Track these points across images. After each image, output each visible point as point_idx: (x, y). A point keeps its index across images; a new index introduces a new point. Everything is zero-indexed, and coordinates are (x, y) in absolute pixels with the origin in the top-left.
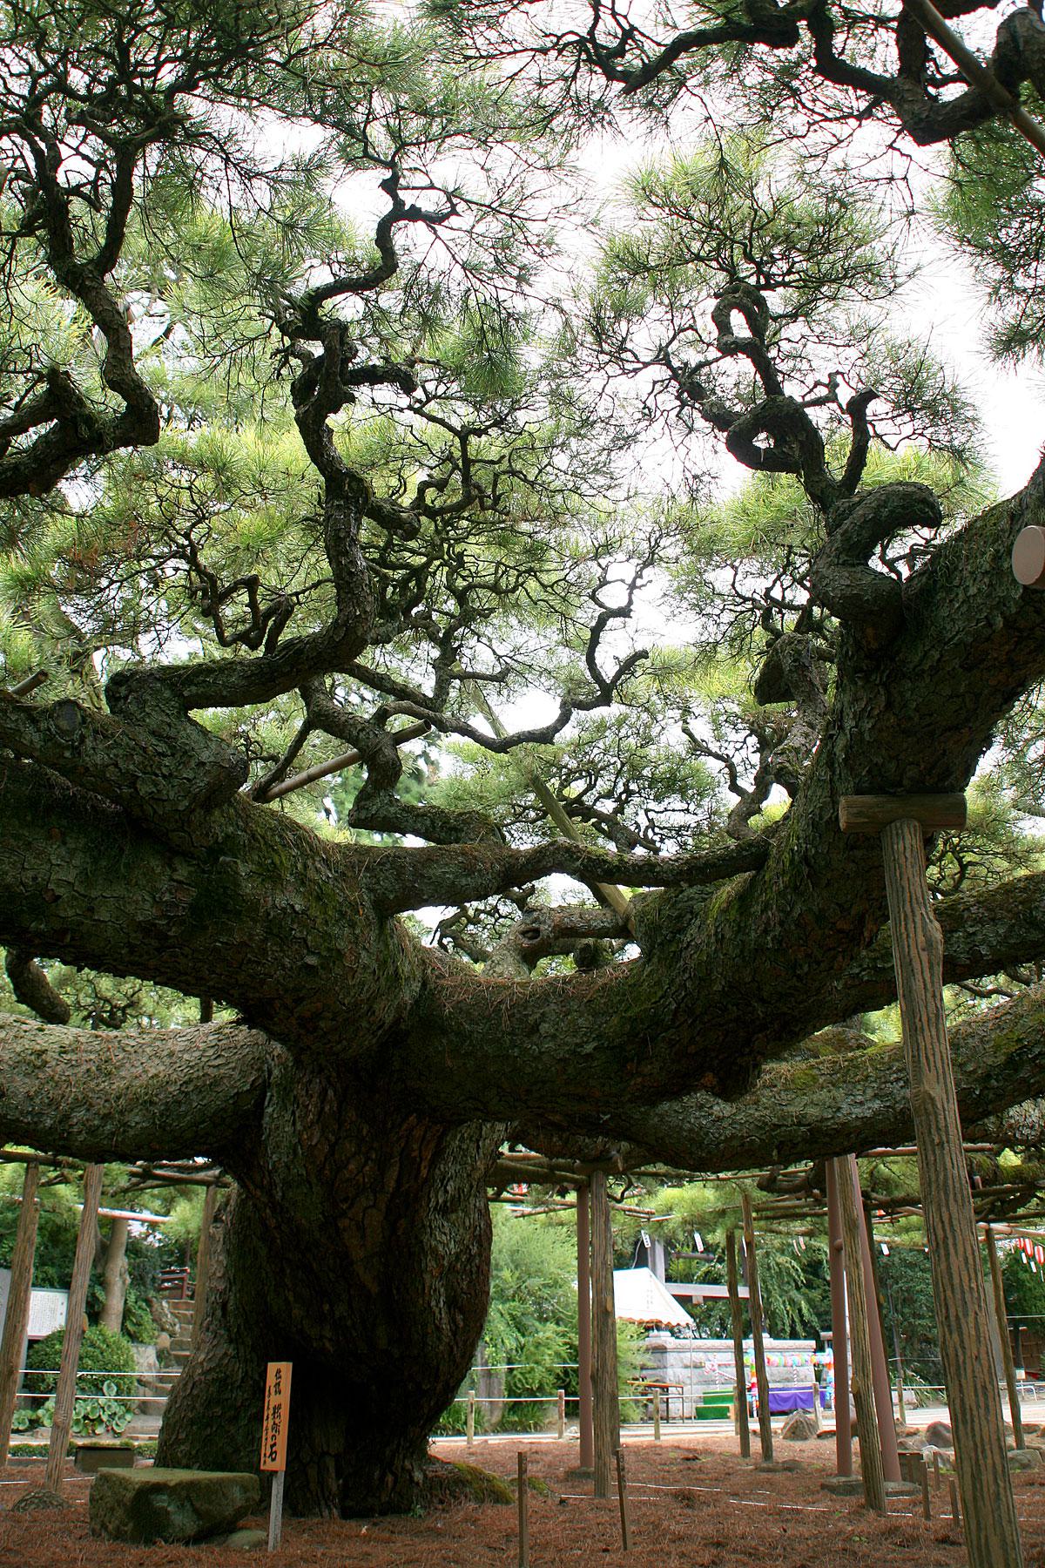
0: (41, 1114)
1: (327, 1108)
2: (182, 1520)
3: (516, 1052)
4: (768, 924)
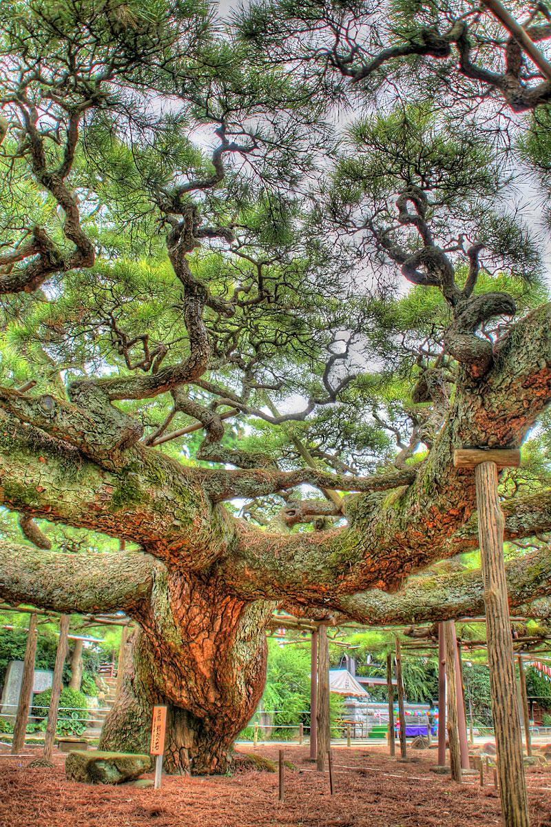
1: (184, 592)
2: (112, 774)
4: (414, 510)
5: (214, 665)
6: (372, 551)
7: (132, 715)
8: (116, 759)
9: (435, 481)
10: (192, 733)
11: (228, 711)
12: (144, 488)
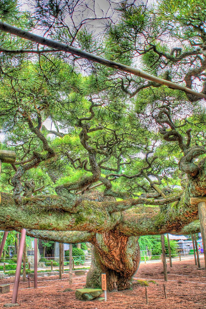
0: (58, 238)
1: (107, 235)
2: (90, 297)
3: (139, 227)
4: (181, 211)
5: (121, 256)
6: (169, 221)
7: (96, 273)
8: (91, 292)
9: (186, 204)
10: (117, 277)
11: (128, 270)
12: (85, 217)
